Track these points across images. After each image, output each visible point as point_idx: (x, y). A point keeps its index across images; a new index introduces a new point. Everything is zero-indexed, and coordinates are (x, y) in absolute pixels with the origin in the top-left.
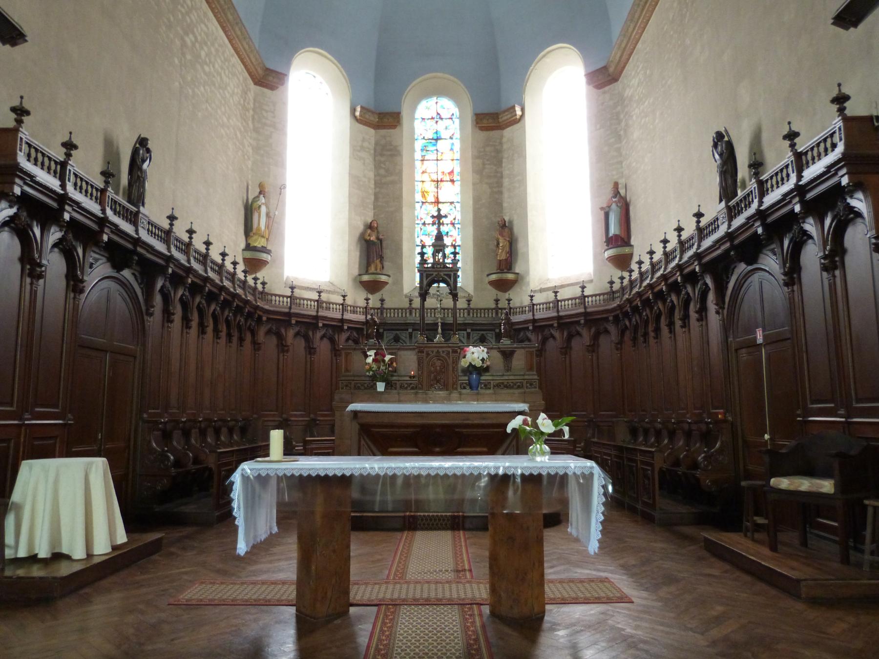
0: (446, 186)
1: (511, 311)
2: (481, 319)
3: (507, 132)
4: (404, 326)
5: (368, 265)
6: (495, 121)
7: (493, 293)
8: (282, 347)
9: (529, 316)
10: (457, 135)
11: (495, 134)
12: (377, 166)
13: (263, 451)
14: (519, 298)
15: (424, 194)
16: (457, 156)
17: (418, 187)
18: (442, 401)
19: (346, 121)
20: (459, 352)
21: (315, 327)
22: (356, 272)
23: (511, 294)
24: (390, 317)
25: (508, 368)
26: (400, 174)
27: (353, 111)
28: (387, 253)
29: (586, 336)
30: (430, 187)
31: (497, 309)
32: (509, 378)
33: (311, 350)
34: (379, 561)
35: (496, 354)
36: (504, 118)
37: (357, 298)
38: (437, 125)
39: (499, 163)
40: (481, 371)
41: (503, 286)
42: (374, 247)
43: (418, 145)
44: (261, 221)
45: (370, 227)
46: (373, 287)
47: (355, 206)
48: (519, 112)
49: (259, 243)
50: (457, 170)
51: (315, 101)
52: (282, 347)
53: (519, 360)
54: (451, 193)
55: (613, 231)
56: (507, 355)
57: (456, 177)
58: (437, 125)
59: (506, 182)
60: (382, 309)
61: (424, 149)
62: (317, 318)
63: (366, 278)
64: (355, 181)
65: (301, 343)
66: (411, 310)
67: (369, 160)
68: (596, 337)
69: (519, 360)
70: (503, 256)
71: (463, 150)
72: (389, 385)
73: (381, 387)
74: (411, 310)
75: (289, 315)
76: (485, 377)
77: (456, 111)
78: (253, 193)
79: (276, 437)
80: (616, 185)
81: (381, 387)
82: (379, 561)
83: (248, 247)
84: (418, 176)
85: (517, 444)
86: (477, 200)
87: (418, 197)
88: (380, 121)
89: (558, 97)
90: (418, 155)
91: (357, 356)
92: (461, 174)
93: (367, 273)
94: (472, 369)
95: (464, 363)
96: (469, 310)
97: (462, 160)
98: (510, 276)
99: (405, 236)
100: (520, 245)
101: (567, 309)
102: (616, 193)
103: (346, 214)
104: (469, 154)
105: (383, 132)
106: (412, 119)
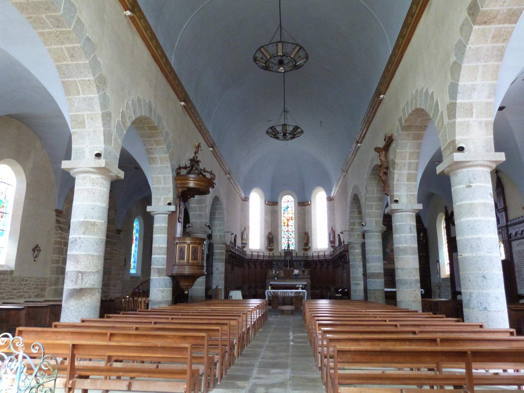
0: (290, 221)
1: (307, 257)
2: (300, 259)
3: (307, 207)
4: (279, 261)
5: (269, 244)
6: (303, 204)
7: (303, 252)
8: (249, 267)
9: (312, 259)
10: (293, 207)
11: (303, 207)
12: (272, 216)
13: (268, 289)
14: (310, 253)
15: (284, 223)
16: (293, 212)
17: (283, 221)
18: (288, 282)
19: (263, 205)
20: (293, 271)
21: (257, 262)
22: (266, 246)
23: (308, 252)
24: (276, 258)
25: (304, 274)
26: (278, 218)
27: (265, 202)
28: (274, 240)
29: (326, 264)
30: (286, 221)
31: (304, 256)
32: (304, 277)
33: (256, 268)
34: (247, 365)
35: (301, 271)
36: (306, 204)
37: (267, 253)
38: (288, 203)
39: (305, 215)
40: (297, 275)
41: (306, 250)
42: (271, 239)
43: (283, 209)
44: (245, 237)
45: (270, 233)
46: (271, 250)
47: (266, 228)
48: (310, 203)
49: (244, 242)
50: (293, 216)
51: (256, 201)
52: (249, 267)
53: (306, 272)
54: (292, 223)
55: (331, 239)
56: (303, 272)
57: (293, 219)
58: (288, 203)
59: (307, 221)
60: (273, 256)
61: (284, 210)
62: (257, 260)
63: (269, 248)
64: (266, 221)
65: (253, 266)
66: (281, 256)
67: (270, 215)
68: (328, 265)
69: (306, 272)
70: (306, 242)
71: (295, 211)
72: (278, 278)
73: (276, 279)
74: (281, 256)
75: (251, 259)
76: (299, 276)
77: (293, 199)
78: (243, 229)
79: (270, 287)
80: (332, 228)
81: (276, 279)
82: (247, 365)
83: (242, 243)
84: (283, 218)
85: (298, 288)
86: (299, 226)
87: (283, 224)
88: (272, 203)
89: (320, 200)
90: (282, 212)
91: (271, 272)
92: (294, 217)
93: (269, 246)
94: (295, 275)
95: (294, 274)
96: (296, 256)
97: (295, 214)
98: (307, 248)
99: (279, 236)
100: (310, 239)
101: (322, 258)
102: (332, 229)
103: (264, 231)
104: (297, 213)
105: (273, 207)
106: (281, 202)
